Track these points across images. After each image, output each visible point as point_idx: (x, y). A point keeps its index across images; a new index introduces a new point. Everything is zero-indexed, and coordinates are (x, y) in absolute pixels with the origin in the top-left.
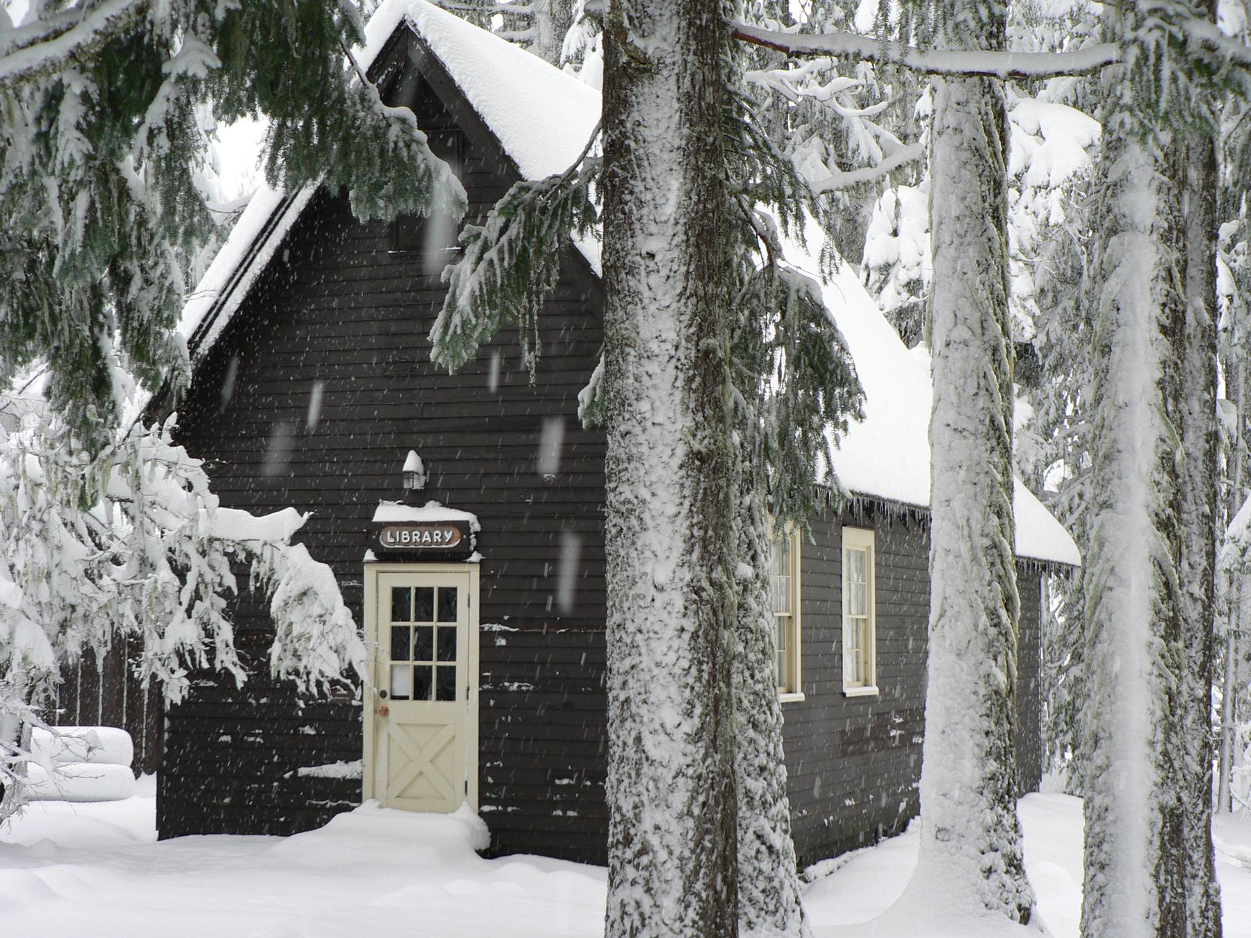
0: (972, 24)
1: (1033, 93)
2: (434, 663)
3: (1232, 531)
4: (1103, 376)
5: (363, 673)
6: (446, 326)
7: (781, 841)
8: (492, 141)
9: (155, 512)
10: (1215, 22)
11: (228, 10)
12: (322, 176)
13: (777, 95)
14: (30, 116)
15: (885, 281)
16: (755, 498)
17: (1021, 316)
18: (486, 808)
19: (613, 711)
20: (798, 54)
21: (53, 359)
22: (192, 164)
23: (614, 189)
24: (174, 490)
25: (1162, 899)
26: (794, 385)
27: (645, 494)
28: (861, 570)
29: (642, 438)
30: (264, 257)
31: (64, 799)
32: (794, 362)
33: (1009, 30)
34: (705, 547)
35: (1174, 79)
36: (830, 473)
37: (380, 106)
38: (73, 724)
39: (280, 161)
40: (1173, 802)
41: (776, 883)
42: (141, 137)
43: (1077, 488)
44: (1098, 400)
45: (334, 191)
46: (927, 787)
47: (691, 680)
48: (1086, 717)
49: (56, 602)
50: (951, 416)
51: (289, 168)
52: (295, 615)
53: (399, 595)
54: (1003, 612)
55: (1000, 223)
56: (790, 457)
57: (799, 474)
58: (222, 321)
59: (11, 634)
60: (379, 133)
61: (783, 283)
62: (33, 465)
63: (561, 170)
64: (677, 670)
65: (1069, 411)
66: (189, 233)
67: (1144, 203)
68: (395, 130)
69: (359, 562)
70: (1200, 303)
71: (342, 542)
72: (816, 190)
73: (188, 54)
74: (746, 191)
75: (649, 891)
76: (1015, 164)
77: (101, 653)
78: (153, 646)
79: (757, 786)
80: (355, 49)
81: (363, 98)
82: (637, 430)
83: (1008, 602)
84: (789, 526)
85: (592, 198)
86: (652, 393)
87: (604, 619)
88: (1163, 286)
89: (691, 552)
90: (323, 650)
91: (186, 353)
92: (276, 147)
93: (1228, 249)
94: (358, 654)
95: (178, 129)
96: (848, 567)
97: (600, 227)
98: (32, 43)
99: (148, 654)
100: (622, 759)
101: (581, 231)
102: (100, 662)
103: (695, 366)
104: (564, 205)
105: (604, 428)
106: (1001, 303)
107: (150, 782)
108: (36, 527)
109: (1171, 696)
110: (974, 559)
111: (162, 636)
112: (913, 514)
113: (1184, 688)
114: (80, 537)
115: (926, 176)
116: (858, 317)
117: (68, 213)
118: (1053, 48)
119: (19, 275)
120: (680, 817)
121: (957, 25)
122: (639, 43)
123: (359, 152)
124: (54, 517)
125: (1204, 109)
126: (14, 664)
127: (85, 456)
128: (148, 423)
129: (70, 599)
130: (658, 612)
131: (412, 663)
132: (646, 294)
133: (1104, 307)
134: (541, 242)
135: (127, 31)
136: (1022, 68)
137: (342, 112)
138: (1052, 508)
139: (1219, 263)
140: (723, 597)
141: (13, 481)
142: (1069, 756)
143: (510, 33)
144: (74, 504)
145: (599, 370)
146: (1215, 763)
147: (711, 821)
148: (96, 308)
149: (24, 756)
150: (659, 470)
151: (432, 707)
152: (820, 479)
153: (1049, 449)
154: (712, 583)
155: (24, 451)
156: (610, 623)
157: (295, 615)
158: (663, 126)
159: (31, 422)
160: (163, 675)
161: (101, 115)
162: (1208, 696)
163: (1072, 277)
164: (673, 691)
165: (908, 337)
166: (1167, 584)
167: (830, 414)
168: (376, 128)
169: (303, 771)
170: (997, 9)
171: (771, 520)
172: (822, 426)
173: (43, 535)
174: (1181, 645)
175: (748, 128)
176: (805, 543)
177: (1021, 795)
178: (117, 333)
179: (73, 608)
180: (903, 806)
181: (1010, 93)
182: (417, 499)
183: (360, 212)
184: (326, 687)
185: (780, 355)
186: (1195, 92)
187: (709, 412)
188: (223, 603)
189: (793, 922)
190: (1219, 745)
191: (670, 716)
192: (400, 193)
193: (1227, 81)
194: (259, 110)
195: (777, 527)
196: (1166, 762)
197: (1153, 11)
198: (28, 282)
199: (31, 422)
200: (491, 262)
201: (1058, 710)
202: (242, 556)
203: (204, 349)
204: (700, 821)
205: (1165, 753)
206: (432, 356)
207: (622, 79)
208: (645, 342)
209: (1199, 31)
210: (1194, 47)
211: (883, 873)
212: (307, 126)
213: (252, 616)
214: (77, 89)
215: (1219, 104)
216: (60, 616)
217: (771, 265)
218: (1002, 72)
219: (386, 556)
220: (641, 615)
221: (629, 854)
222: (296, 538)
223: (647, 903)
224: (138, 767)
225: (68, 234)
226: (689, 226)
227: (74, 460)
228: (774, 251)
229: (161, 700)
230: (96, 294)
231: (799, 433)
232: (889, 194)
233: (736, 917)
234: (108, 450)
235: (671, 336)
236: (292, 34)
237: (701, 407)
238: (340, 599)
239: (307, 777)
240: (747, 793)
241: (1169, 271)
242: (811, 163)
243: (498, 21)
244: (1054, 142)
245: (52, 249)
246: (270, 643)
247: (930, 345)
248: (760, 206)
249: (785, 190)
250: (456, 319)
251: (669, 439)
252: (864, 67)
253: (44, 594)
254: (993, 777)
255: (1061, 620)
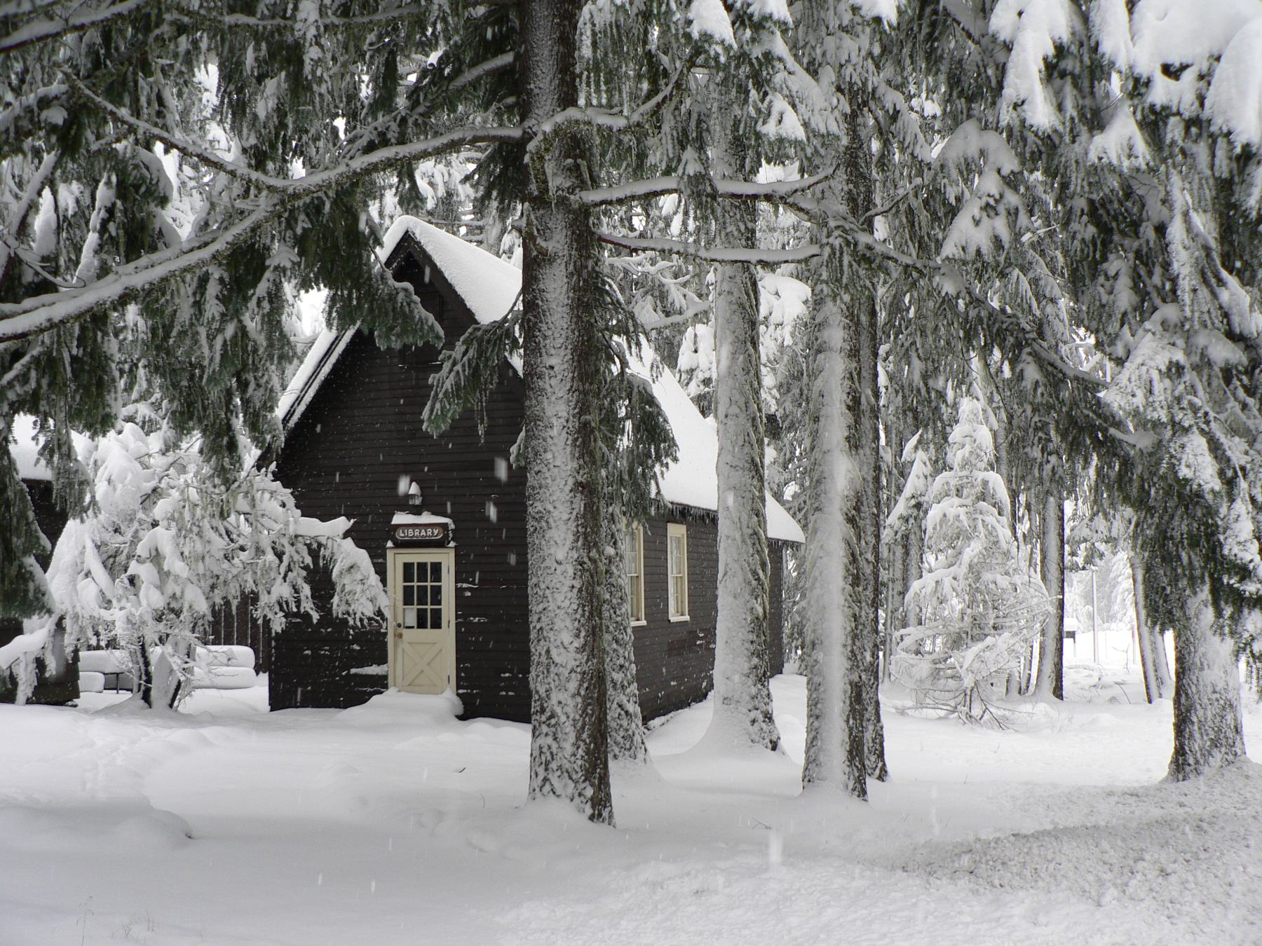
0: (736, 233)
1: (773, 271)
2: (429, 607)
3: (888, 521)
4: (815, 435)
5: (387, 614)
6: (432, 411)
7: (633, 708)
8: (460, 302)
9: (264, 520)
10: (873, 233)
11: (304, 229)
12: (358, 323)
13: (626, 272)
14: (190, 291)
15: (691, 379)
16: (616, 509)
17: (769, 398)
18: (461, 691)
19: (533, 635)
20: (636, 250)
21: (204, 432)
22: (284, 317)
23: (530, 330)
24: (275, 507)
25: (851, 734)
26: (637, 442)
27: (550, 507)
28: (678, 548)
29: (547, 475)
30: (327, 369)
31: (214, 687)
32: (636, 429)
33: (758, 235)
34: (585, 538)
35: (851, 266)
36: (658, 493)
37: (391, 282)
38: (219, 644)
39: (334, 314)
40: (857, 679)
41: (630, 732)
42: (252, 304)
43: (803, 498)
44: (812, 449)
45: (366, 332)
46: (717, 674)
47: (578, 616)
48: (808, 630)
49: (208, 573)
50: (729, 458)
51: (339, 318)
52: (346, 580)
53: (408, 567)
54: (760, 572)
55: (755, 344)
56: (636, 485)
57: (642, 495)
58: (302, 408)
59: (182, 592)
60: (392, 297)
61: (629, 382)
62: (193, 494)
63: (499, 318)
64: (570, 611)
65: (797, 453)
66: (281, 358)
67: (836, 336)
68: (401, 296)
69: (385, 549)
70: (870, 392)
71: (373, 537)
72: (648, 328)
73: (281, 254)
74: (607, 329)
75: (555, 739)
76: (763, 311)
77: (235, 603)
78: (264, 599)
79: (618, 676)
80: (378, 249)
81: (383, 277)
82: (545, 470)
83: (763, 565)
84: (635, 524)
85: (517, 334)
86: (553, 448)
87: (527, 580)
88: (847, 383)
89: (577, 541)
90: (363, 600)
91: (281, 427)
92: (331, 308)
93: (885, 360)
94: (384, 602)
95: (275, 298)
96: (671, 546)
97: (522, 351)
98: (192, 250)
99: (261, 603)
100: (538, 663)
101: (511, 353)
102: (234, 608)
103: (579, 432)
104: (500, 338)
105: (525, 468)
106: (757, 392)
107: (264, 678)
108: (195, 529)
109: (855, 617)
110: (744, 541)
111: (269, 593)
112: (708, 515)
113: (863, 613)
114: (221, 535)
115: (712, 317)
116: (674, 400)
117: (211, 347)
118: (783, 247)
119: (185, 383)
120: (573, 696)
121: (727, 234)
122: (543, 244)
123: (380, 309)
124: (206, 524)
125: (868, 284)
126: (185, 610)
127: (223, 488)
128: (259, 468)
129: (216, 572)
130: (558, 577)
131: (415, 607)
132: (549, 390)
133: (814, 395)
134: (487, 360)
135: (245, 242)
136: (765, 258)
137: (370, 286)
138: (788, 510)
139: (880, 369)
140: (597, 567)
141: (182, 503)
142: (799, 652)
143: (470, 237)
144: (217, 517)
145: (522, 434)
146: (881, 654)
147: (591, 698)
148: (229, 400)
149: (191, 664)
150: (558, 493)
151: (429, 633)
152: (653, 496)
153: (786, 476)
154: (590, 559)
155: (188, 486)
156: (530, 583)
157: (346, 580)
158: (558, 291)
159: (192, 468)
160: (270, 616)
161: (230, 290)
162: (877, 617)
163: (798, 377)
164: (568, 623)
165: (704, 412)
166: (853, 554)
167: (658, 458)
168: (390, 295)
169: (353, 671)
170: (750, 225)
171: (624, 520)
172: (653, 466)
173: (200, 534)
174: (861, 589)
175: (607, 292)
176: (645, 533)
177: (771, 677)
178: (241, 415)
179: (218, 577)
180: (704, 684)
181: (759, 271)
182: (417, 511)
183: (381, 345)
184: (366, 621)
185: (629, 425)
186: (862, 272)
187: (587, 459)
188: (304, 573)
189: (641, 755)
190: (884, 643)
191: (566, 637)
192: (404, 332)
193: (880, 267)
194: (322, 286)
195: (628, 525)
196: (853, 657)
197: (837, 227)
198: (189, 387)
199: (192, 468)
200: (458, 372)
201: (793, 627)
202: (315, 546)
203: (291, 424)
204: (585, 698)
205: (852, 651)
206: (424, 427)
207: (533, 266)
208: (549, 418)
209: (863, 238)
210: (860, 247)
211: (693, 725)
212: (350, 294)
213: (321, 579)
214: (217, 276)
215: (875, 280)
216: (210, 582)
217: (622, 373)
218: (754, 260)
219: (400, 545)
220: (549, 578)
221: (544, 718)
222: (346, 535)
223: (554, 746)
224: (258, 669)
225: (212, 360)
226: (574, 350)
227: (217, 491)
228: (624, 364)
229: (270, 630)
230: (229, 394)
231: (640, 470)
232: (690, 329)
233: (606, 753)
234: (236, 484)
235: (565, 414)
236: (341, 241)
237: (582, 456)
238: (373, 570)
239: (356, 675)
240: (612, 681)
241: (851, 374)
242: (646, 313)
243: (463, 230)
244: (785, 298)
245: (202, 368)
246: (332, 596)
247: (716, 417)
248: (615, 338)
249: (631, 329)
250: (438, 406)
251: (563, 474)
252: (675, 256)
253: (201, 570)
254: (755, 667)
255: (795, 574)
